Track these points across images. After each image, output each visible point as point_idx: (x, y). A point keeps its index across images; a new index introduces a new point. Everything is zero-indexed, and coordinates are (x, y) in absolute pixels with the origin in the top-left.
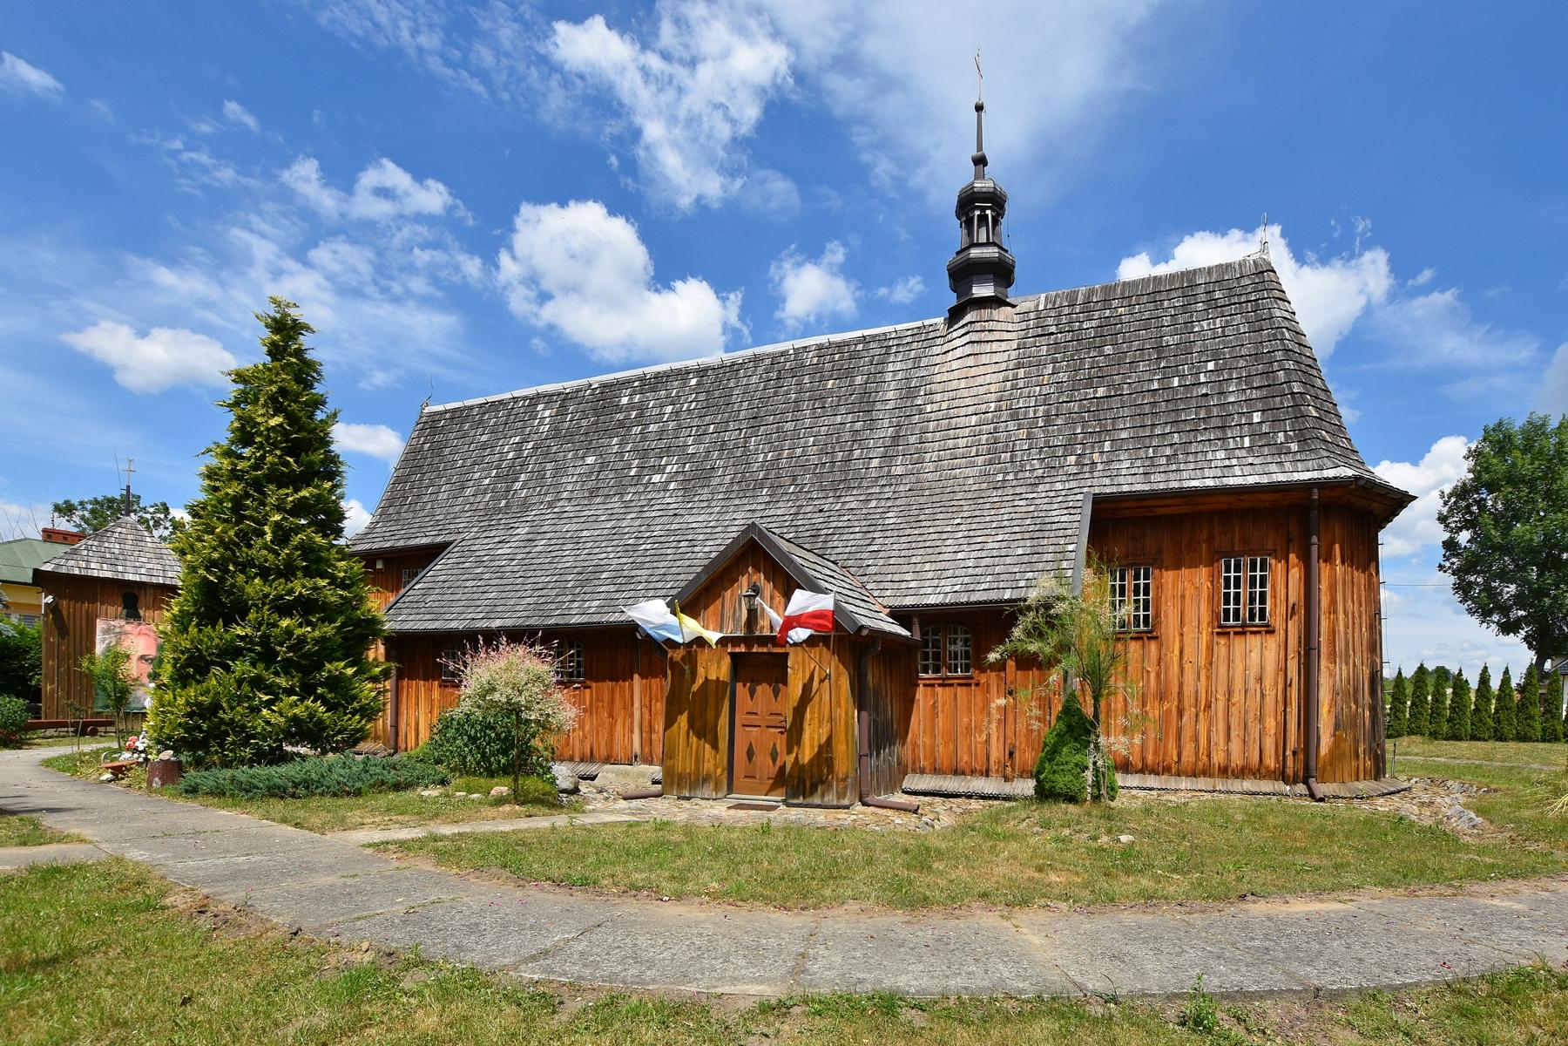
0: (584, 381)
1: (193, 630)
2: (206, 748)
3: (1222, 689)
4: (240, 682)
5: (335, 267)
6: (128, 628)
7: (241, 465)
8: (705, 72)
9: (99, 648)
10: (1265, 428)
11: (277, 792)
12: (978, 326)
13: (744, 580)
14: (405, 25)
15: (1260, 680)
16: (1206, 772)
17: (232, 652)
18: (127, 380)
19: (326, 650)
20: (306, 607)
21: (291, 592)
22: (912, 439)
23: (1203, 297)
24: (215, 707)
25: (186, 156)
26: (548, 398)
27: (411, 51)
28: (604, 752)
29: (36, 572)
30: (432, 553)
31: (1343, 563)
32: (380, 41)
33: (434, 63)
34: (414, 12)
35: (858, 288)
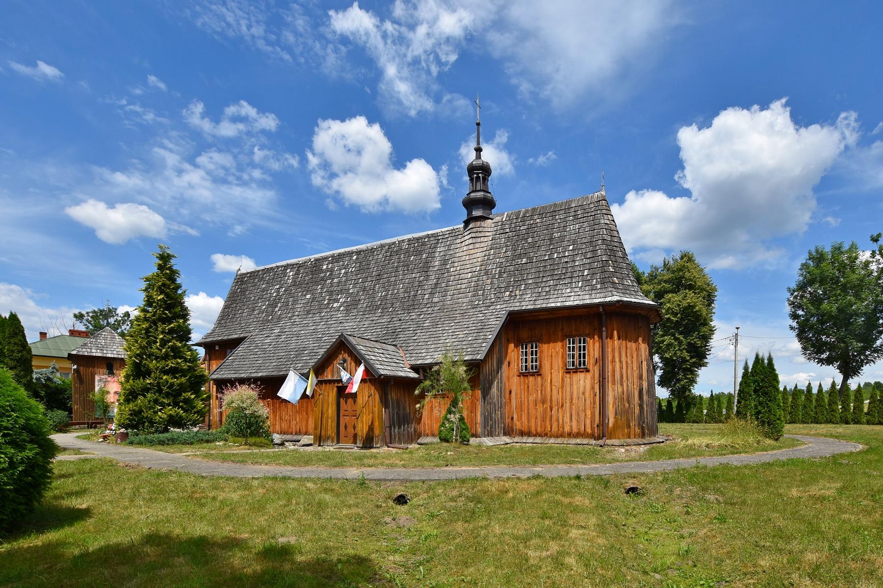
0: (307, 258)
1: (131, 381)
2: (137, 426)
3: (568, 398)
4: (149, 401)
5: (211, 167)
6: (109, 379)
7: (148, 315)
8: (422, 30)
9: (97, 389)
10: (589, 278)
11: (162, 443)
12: (475, 230)
13: (341, 357)
14: (243, 23)
15: (584, 393)
16: (562, 436)
17: (145, 390)
18: (104, 235)
19: (182, 388)
20: (173, 372)
21: (168, 365)
22: (443, 285)
23: (573, 214)
24: (141, 411)
25: (128, 108)
26: (291, 266)
27: (248, 38)
28: (304, 430)
29: (69, 354)
30: (238, 342)
31: (619, 339)
32: (231, 33)
33: (261, 44)
34: (248, 14)
35: (516, 159)
